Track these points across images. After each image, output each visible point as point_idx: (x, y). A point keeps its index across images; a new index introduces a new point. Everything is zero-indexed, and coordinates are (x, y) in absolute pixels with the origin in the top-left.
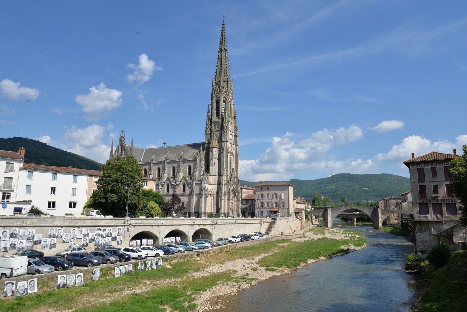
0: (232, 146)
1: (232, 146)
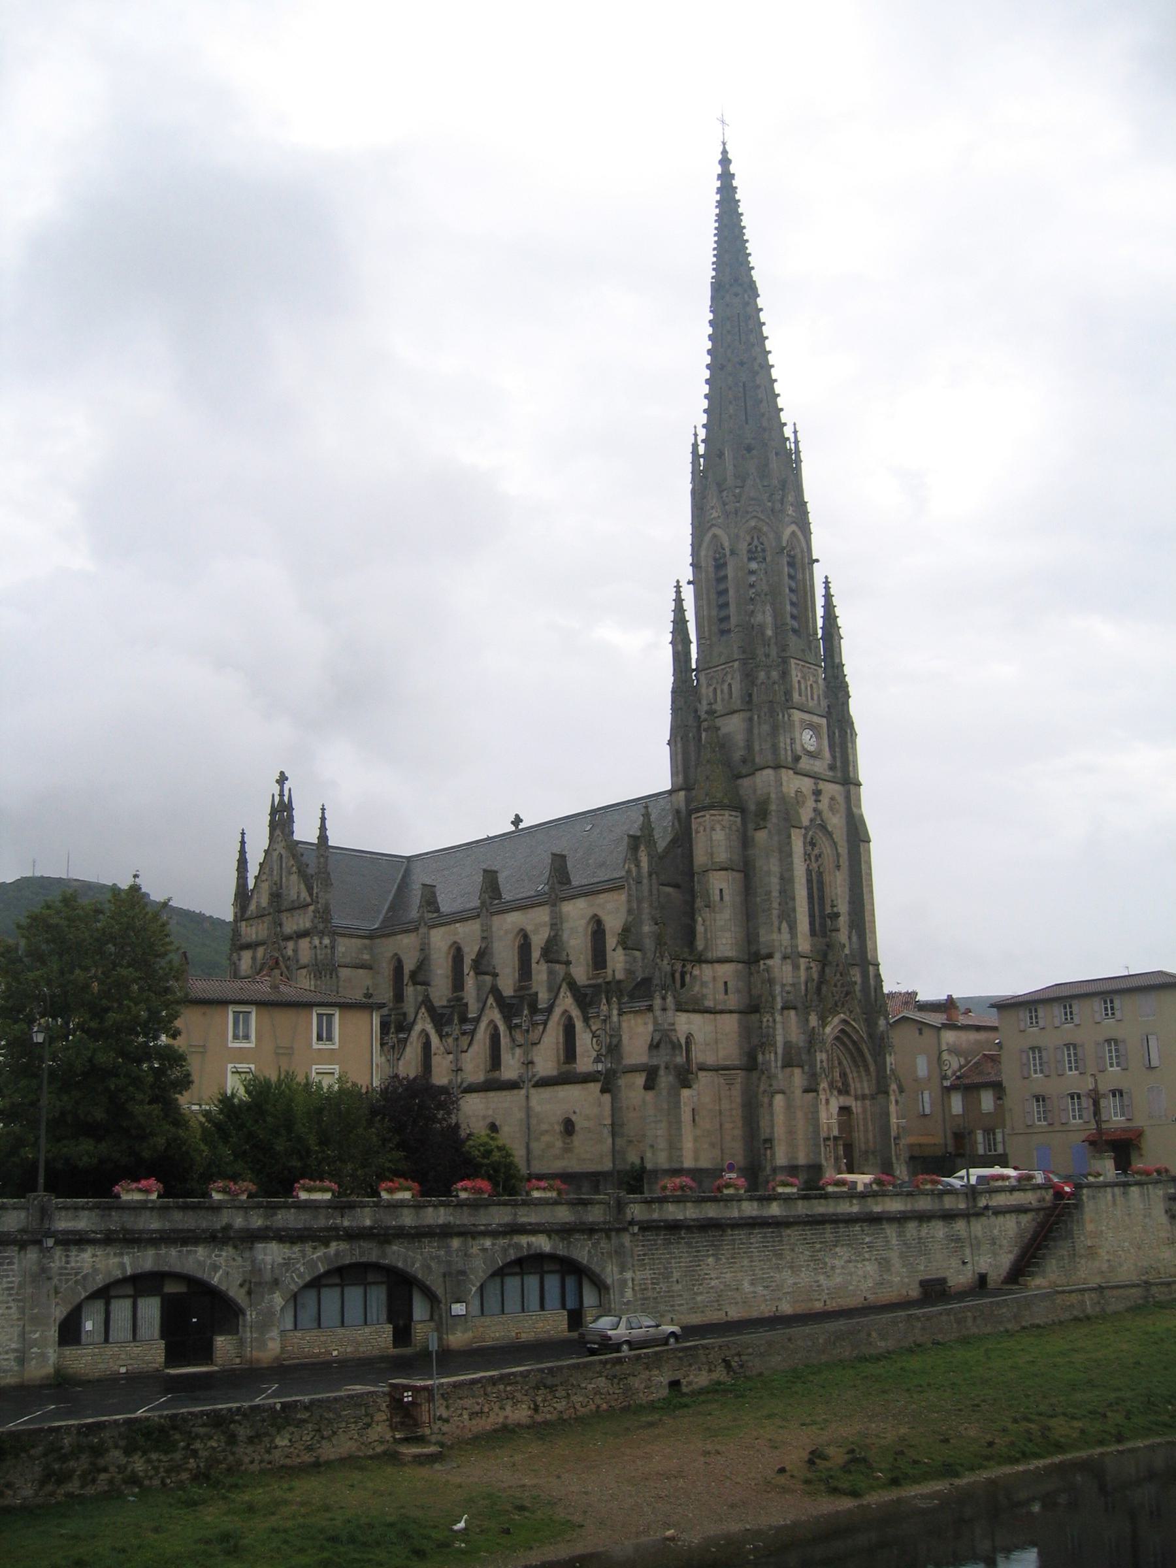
0: (817, 793)
1: (817, 793)
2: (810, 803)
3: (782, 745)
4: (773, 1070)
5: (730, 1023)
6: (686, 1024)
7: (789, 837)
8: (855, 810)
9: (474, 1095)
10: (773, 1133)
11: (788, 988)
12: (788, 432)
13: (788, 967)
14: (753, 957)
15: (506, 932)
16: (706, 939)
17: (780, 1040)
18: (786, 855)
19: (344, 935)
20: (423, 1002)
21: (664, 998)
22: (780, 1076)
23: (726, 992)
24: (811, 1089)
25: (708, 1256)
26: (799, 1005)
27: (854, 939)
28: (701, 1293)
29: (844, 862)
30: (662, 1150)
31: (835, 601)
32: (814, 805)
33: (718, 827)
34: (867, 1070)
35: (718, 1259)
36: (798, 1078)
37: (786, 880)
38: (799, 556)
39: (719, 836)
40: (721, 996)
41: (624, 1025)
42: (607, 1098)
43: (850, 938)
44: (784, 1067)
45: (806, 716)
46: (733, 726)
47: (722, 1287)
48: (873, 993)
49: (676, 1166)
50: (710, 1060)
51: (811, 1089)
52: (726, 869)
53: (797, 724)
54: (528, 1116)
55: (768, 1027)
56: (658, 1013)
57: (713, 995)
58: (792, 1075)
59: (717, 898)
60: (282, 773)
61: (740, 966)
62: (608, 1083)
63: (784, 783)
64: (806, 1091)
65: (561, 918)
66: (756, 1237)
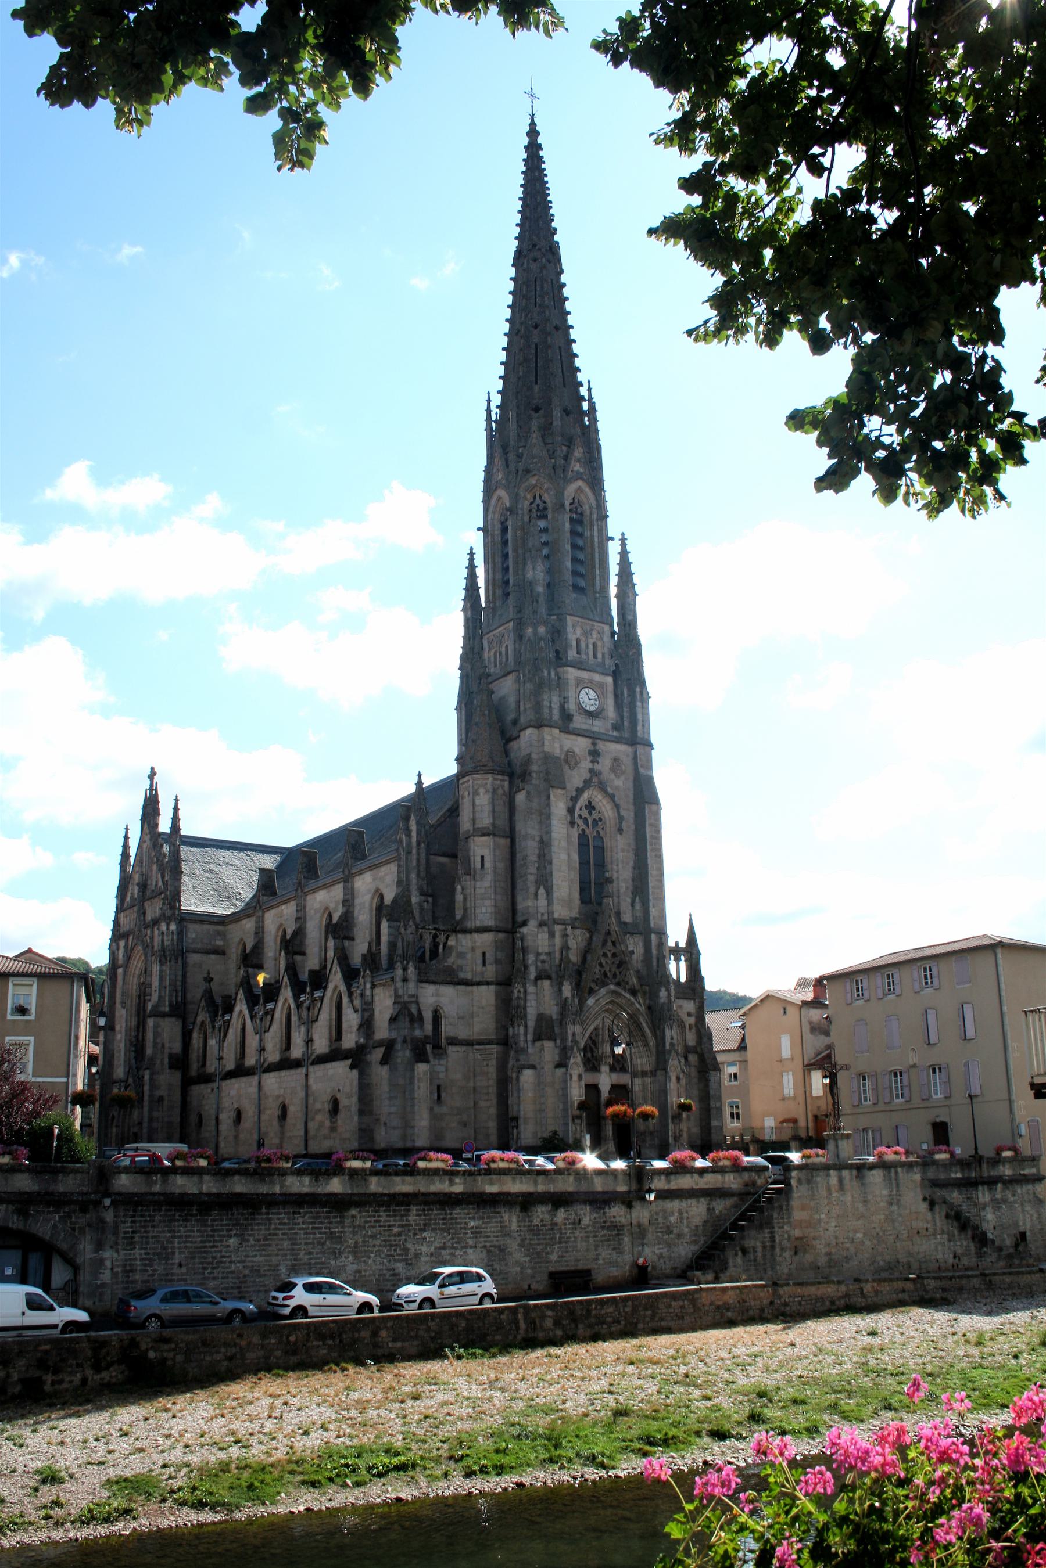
0: (595, 754)
1: (595, 754)
2: (586, 764)
3: (546, 703)
4: (522, 1044)
5: (486, 995)
6: (431, 996)
7: (548, 797)
8: (642, 771)
9: (272, 1074)
10: (519, 1111)
11: (543, 957)
12: (583, 391)
13: (543, 936)
14: (511, 924)
15: (316, 911)
16: (465, 910)
17: (532, 1012)
18: (545, 817)
19: (195, 921)
20: (242, 984)
21: (405, 969)
22: (530, 1050)
23: (484, 964)
24: (562, 1064)
25: (230, 1237)
26: (554, 976)
27: (638, 906)
28: (214, 1278)
29: (629, 825)
30: (394, 1128)
31: (631, 558)
32: (590, 765)
33: (482, 791)
34: (646, 1045)
35: (243, 1240)
36: (549, 1050)
37: (545, 844)
38: (588, 512)
39: (483, 800)
40: (479, 968)
41: (376, 998)
42: (355, 1072)
43: (633, 905)
44: (534, 1041)
45: (585, 675)
46: (506, 688)
47: (247, 1272)
48: (655, 964)
49: (409, 1145)
50: (463, 1034)
51: (562, 1064)
52: (488, 835)
53: (572, 682)
54: (307, 1095)
55: (518, 998)
56: (399, 984)
57: (471, 967)
58: (542, 1049)
59: (478, 865)
60: (152, 769)
61: (501, 935)
62: (357, 1058)
63: (546, 743)
64: (558, 1066)
65: (353, 894)
66: (304, 1219)
